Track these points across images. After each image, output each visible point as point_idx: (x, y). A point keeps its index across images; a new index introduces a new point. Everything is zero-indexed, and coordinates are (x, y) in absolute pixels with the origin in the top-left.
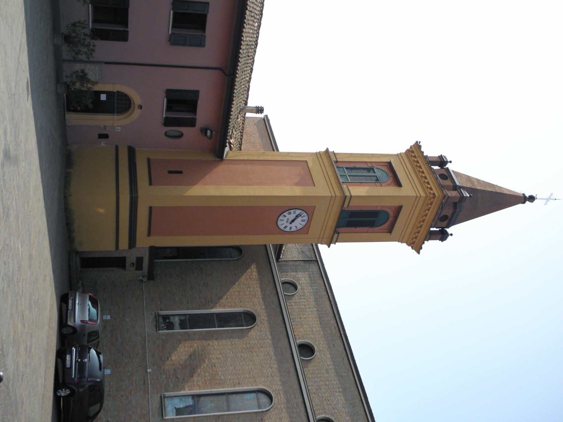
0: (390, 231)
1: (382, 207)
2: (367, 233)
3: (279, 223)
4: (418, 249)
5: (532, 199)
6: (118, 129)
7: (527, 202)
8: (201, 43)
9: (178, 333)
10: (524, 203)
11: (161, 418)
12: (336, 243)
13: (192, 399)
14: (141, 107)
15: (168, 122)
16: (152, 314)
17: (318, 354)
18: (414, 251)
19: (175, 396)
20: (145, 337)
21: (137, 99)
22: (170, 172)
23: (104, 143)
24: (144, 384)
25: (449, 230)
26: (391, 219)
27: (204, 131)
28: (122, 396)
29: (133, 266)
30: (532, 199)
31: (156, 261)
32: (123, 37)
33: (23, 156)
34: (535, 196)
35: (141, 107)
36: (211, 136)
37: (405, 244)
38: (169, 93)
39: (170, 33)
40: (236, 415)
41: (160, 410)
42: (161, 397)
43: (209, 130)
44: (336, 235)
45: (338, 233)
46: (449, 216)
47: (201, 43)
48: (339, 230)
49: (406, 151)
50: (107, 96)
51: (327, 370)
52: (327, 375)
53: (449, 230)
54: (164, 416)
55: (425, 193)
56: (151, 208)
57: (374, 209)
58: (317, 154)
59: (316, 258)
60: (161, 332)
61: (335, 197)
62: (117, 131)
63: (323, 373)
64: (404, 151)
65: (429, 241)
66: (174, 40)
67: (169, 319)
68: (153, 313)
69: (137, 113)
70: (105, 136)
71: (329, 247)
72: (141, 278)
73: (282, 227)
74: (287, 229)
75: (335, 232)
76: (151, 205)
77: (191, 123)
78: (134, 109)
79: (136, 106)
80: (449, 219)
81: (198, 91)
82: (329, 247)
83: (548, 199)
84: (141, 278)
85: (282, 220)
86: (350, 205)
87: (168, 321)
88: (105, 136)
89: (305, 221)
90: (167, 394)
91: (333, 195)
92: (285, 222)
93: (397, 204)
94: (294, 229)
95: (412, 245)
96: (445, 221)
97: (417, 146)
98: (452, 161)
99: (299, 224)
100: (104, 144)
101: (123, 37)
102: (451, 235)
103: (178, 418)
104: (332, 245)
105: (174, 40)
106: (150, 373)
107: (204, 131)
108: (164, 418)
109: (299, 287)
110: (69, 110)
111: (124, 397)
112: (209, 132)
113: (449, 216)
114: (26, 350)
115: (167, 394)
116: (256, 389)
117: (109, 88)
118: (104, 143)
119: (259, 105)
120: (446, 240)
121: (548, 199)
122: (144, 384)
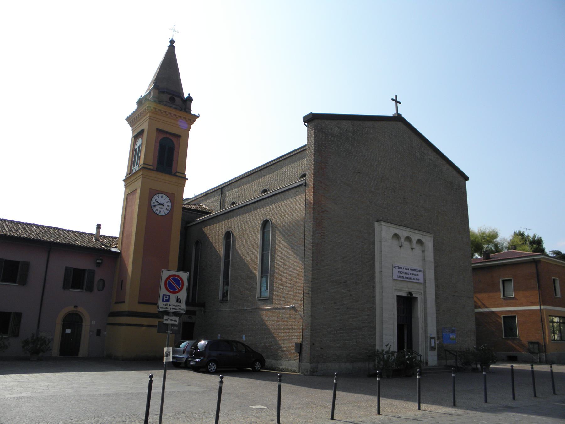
0: (178, 137)
1: (156, 142)
2: (179, 153)
3: (162, 213)
4: (196, 117)
5: (172, 42)
6: (94, 322)
7: (174, 45)
8: (27, 265)
9: (231, 287)
10: (174, 47)
11: (268, 300)
12: (186, 174)
13: (263, 278)
14: (76, 307)
15: (90, 289)
16: (220, 305)
17: (267, 187)
18: (197, 120)
19: (260, 290)
20: (230, 310)
21: (71, 308)
22: (121, 289)
23: (104, 332)
24: (251, 312)
25: (186, 96)
26: (168, 136)
27: (99, 265)
28: (256, 327)
29: (191, 317)
30: (172, 42)
31: (196, 302)
32: (19, 315)
33: (496, 421)
34: (170, 40)
35: (76, 307)
36: (100, 260)
37: (192, 126)
38: (65, 286)
39: (17, 285)
40: (272, 246)
41: (265, 301)
42: (259, 300)
43: (97, 260)
44: (178, 174)
45: (177, 172)
46: (170, 96)
47: (27, 265)
48: (173, 172)
49: (131, 126)
50: (71, 331)
51: (276, 181)
52: (278, 180)
53: (186, 96)
54: (267, 298)
55: (148, 113)
56: (139, 303)
57: (158, 148)
58: (126, 187)
59: (220, 188)
60: (228, 299)
61: (143, 175)
62: (95, 324)
63: (277, 183)
64: (131, 128)
65: (191, 109)
66: (23, 282)
67: (225, 293)
68: (220, 304)
69: (81, 309)
70: (99, 333)
71: (187, 179)
72: (202, 312)
73: (166, 212)
74: (169, 208)
75: (175, 175)
76: (138, 302)
77: (92, 272)
78: (77, 311)
79: (75, 309)
80: (173, 96)
81: (66, 268)
82: (187, 179)
83: (174, 31)
84: (202, 312)
85: (160, 211)
86: (152, 165)
87: (225, 294)
88: (99, 333)
89: (163, 196)
90: (258, 295)
91: (141, 176)
92: (162, 210)
93: (155, 133)
94: (169, 204)
95: (192, 121)
96: (175, 99)
97: (126, 119)
98: (391, 99)
99: (164, 200)
100: (105, 332)
101: (19, 315)
102: (189, 94)
103: (269, 288)
104: (186, 177)
105: (23, 282)
106: (247, 308)
107: (99, 265)
108: (268, 298)
109: (234, 201)
110: (77, 355)
111: (257, 326)
112: (98, 261)
113: (170, 96)
114: (95, 385)
115: (258, 295)
116: (262, 232)
117: (58, 328)
118: (104, 332)
119: (95, 227)
120: (192, 98)
121: (174, 31)
122: (251, 312)
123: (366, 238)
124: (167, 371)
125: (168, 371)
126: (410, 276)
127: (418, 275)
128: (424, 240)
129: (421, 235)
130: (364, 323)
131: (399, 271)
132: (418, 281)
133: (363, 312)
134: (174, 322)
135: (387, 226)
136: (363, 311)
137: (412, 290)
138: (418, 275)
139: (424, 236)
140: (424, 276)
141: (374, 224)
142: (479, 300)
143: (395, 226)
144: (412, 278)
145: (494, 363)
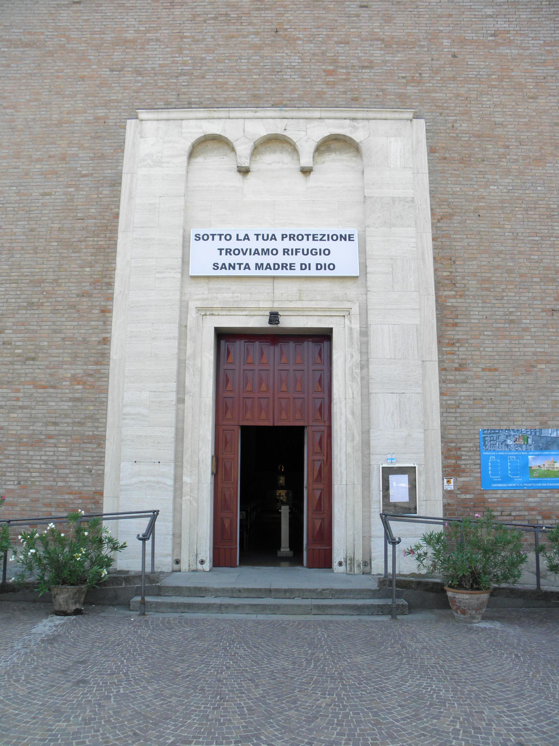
123: (84, 172)
124: (141, 570)
125: (140, 569)
126: (281, 259)
127: (327, 252)
128: (358, 136)
129: (347, 122)
130: (55, 424)
131: (221, 250)
132: (328, 273)
133: (51, 390)
134: (318, 469)
135: (168, 120)
136: (54, 387)
137: (276, 305)
138: (327, 252)
139: (361, 124)
140: (363, 251)
141: (124, 128)
142: (163, 278)
143: (202, 113)
144: (262, 264)
145: (149, 595)
